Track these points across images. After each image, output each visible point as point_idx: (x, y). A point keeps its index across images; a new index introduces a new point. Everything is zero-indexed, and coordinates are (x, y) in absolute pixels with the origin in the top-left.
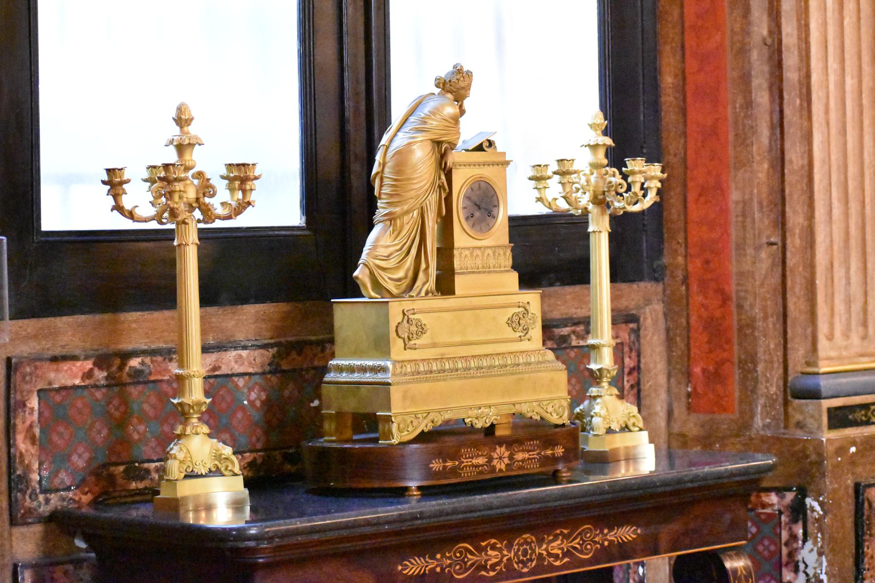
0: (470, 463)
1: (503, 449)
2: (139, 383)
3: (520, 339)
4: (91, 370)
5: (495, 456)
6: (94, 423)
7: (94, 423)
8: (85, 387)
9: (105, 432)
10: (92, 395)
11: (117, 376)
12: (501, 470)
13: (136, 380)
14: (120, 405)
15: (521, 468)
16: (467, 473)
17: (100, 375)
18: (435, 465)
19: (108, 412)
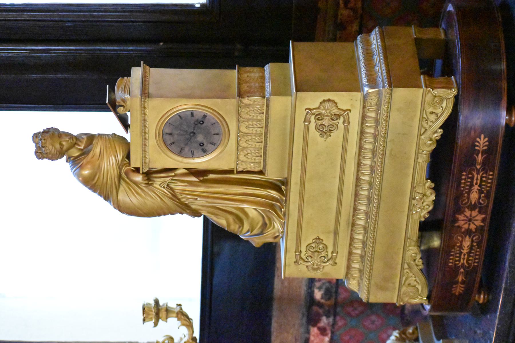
0: (466, 256)
1: (461, 217)
2: (336, 292)
3: (347, 123)
4: (319, 329)
5: (466, 226)
6: (364, 326)
7: (364, 326)
8: (332, 333)
9: (373, 318)
10: (340, 327)
11: (327, 308)
12: (483, 220)
13: (334, 295)
14: (353, 306)
15: (487, 196)
16: (476, 259)
17: (324, 321)
18: (458, 290)
19: (357, 316)
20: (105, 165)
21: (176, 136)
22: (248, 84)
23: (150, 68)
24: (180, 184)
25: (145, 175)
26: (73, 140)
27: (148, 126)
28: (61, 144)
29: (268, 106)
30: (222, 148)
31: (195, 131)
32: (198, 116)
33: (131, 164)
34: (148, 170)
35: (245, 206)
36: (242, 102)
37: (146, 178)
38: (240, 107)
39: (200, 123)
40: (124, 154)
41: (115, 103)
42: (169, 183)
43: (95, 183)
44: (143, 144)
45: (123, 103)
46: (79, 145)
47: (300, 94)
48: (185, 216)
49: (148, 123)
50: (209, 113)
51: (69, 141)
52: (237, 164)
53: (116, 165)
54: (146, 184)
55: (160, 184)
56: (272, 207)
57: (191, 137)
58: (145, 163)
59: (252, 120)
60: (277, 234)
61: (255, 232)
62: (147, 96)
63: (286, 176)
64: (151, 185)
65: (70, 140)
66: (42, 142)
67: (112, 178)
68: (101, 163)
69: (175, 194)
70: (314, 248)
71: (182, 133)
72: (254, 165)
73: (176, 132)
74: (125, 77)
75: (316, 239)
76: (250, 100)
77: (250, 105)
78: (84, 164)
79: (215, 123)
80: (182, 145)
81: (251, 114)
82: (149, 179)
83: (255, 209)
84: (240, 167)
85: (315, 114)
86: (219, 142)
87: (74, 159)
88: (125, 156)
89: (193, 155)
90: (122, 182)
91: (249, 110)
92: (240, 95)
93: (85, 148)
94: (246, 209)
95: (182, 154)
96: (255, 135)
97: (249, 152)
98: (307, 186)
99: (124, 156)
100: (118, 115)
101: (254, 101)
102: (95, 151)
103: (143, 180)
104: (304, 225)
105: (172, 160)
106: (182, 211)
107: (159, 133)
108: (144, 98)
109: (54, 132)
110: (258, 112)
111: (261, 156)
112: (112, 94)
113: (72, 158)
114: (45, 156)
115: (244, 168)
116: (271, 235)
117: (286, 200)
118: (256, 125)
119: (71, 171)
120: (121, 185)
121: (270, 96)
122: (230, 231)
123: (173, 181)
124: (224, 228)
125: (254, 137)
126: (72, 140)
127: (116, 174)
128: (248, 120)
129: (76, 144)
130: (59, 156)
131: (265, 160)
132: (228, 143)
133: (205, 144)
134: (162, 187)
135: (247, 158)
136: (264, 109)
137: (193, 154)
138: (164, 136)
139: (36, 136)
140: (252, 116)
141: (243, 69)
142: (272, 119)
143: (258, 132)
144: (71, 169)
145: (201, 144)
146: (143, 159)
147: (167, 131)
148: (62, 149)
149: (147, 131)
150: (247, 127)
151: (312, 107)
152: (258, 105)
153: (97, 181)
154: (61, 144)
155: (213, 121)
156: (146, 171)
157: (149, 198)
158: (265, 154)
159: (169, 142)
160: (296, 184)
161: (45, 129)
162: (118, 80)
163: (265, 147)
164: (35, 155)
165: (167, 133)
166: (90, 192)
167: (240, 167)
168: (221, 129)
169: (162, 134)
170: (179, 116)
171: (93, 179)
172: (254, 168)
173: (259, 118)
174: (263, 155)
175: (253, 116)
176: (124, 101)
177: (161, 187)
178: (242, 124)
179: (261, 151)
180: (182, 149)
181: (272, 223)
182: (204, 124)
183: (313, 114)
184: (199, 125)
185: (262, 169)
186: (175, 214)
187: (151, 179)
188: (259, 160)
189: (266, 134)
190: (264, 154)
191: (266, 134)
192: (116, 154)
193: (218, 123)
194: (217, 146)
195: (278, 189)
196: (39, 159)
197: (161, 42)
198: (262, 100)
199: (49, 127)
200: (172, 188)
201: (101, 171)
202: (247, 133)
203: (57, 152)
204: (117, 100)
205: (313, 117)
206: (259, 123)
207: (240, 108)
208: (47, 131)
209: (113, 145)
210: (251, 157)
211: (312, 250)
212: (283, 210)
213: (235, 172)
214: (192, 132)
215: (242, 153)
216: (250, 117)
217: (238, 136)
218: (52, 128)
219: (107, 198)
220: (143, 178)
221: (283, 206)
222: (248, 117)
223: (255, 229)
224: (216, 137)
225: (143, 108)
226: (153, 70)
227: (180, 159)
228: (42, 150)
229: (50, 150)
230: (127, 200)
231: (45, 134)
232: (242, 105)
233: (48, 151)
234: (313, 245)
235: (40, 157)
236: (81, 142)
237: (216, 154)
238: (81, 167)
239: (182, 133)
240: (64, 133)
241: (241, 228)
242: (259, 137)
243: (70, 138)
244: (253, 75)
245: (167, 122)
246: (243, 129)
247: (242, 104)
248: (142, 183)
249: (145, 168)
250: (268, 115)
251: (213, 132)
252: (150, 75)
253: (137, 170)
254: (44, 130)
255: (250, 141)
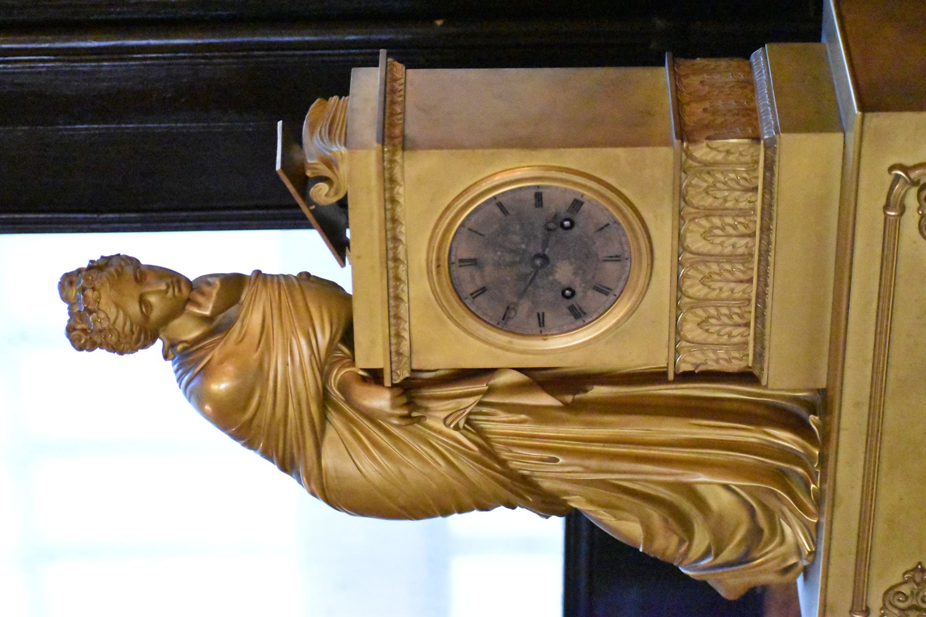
20: (277, 362)
21: (488, 269)
22: (707, 105)
23: (408, 67)
24: (502, 416)
25: (398, 391)
26: (180, 290)
27: (403, 238)
28: (142, 301)
29: (769, 167)
30: (634, 298)
31: (547, 251)
32: (557, 203)
33: (357, 359)
34: (407, 375)
35: (699, 478)
36: (690, 156)
37: (404, 400)
38: (685, 172)
39: (562, 225)
40: (334, 330)
41: (304, 174)
42: (470, 413)
43: (251, 420)
44: (392, 295)
45: (326, 172)
46: (199, 305)
47: (876, 120)
48: (521, 513)
49: (403, 229)
50: (588, 194)
51: (166, 291)
52: (677, 352)
53: (311, 360)
54: (402, 417)
55: (446, 418)
56: (780, 477)
57: (537, 269)
58: (399, 354)
59: (722, 212)
60: (792, 561)
61: (727, 555)
62: (400, 147)
63: (822, 384)
64: (419, 420)
65: (171, 290)
66: (85, 296)
67: (299, 404)
68: (266, 359)
69: (491, 446)
70: (907, 598)
71: (508, 258)
72: (727, 352)
73: (489, 256)
74: (332, 96)
75: (915, 569)
76: (716, 149)
77: (715, 163)
78: (216, 359)
79: (607, 225)
80: (511, 298)
81: (719, 194)
82: (411, 404)
83: (727, 487)
84: (684, 361)
85: (918, 181)
86: (621, 284)
87: (185, 349)
88: (338, 337)
89: (542, 328)
90: (335, 419)
91: (711, 180)
92: (684, 134)
93: (216, 312)
94: (701, 489)
95: (511, 322)
96: (731, 258)
97: (712, 311)
98: (890, 412)
99: (335, 336)
100: (313, 207)
101: (728, 152)
102: (247, 321)
103: (394, 406)
104: (881, 530)
105: (478, 344)
106: (513, 498)
107: (438, 259)
108: (389, 151)
109: (121, 266)
110: (738, 187)
111: (747, 325)
112: (296, 147)
113: (180, 347)
114: (97, 339)
115: (698, 362)
116: (776, 561)
117: (823, 459)
118: (734, 227)
119: (177, 385)
120: (328, 424)
121: (777, 132)
122: (652, 555)
123: (485, 410)
124: (635, 547)
125: (728, 267)
126: (176, 290)
127: (312, 390)
128: (709, 213)
129: (189, 301)
130: (138, 340)
131: (760, 338)
132: (648, 285)
133: (578, 290)
134: (452, 426)
135: (707, 331)
136: (757, 178)
137: (542, 323)
138: (454, 268)
139: (68, 281)
140: (721, 201)
141: (686, 65)
142: (781, 210)
143: (740, 251)
144: (178, 380)
145: (567, 292)
146: (393, 341)
147: (464, 253)
148: (146, 317)
149: (402, 256)
150: (707, 235)
151: (909, 162)
152: (742, 164)
153: (255, 415)
154: (142, 301)
155: (604, 220)
156: (402, 378)
157: (412, 462)
158: (760, 316)
159: (470, 289)
160: (857, 405)
161: (96, 258)
162: (313, 106)
163: (761, 296)
164: (68, 336)
165: (461, 261)
166: (236, 447)
167: (684, 361)
168: (627, 242)
169: (446, 264)
170: (500, 205)
171: (245, 408)
172: (729, 361)
173: (743, 205)
174: (756, 322)
175: (725, 200)
176: (330, 163)
177: (448, 426)
178: (692, 227)
179: (747, 309)
180: (508, 308)
181: (778, 523)
182: (576, 230)
183: (914, 183)
184: (560, 230)
185: (750, 365)
186: (493, 509)
187: (419, 402)
188: (742, 336)
189: (764, 254)
190: (756, 318)
191: (764, 254)
192: (311, 331)
193: (619, 224)
194: (614, 297)
195: (799, 426)
196: (80, 349)
197: (438, 18)
198: (751, 146)
199: (107, 254)
200: (482, 428)
201: (268, 379)
202: (706, 255)
203: (132, 326)
204: (309, 161)
205: (914, 191)
206: (742, 220)
207: (683, 175)
208: (100, 263)
209: (301, 303)
210: (718, 328)
211: (901, 605)
212: (813, 486)
213: (671, 376)
214: (538, 256)
215: (689, 317)
216: (716, 204)
217: (679, 263)
218: (119, 255)
219: (287, 465)
220: (393, 398)
221: (814, 475)
222: (708, 201)
223: (728, 545)
224: (611, 268)
225: (389, 181)
226: (415, 75)
227: (502, 338)
228: (87, 322)
229: (112, 318)
230: (348, 467)
231: (94, 273)
232: (690, 167)
233: (105, 324)
234: (906, 589)
235: (83, 341)
236: (202, 294)
237: (614, 321)
238: (206, 372)
239: (508, 258)
240: (151, 268)
241: (687, 544)
242: (743, 264)
243: (172, 282)
244: (717, 79)
245: (462, 225)
246: (695, 242)
247: (690, 162)
248: (391, 416)
249: (397, 369)
250: (771, 193)
251: (602, 254)
252: (409, 88)
253: (375, 377)
254: (92, 261)
255: (716, 277)
